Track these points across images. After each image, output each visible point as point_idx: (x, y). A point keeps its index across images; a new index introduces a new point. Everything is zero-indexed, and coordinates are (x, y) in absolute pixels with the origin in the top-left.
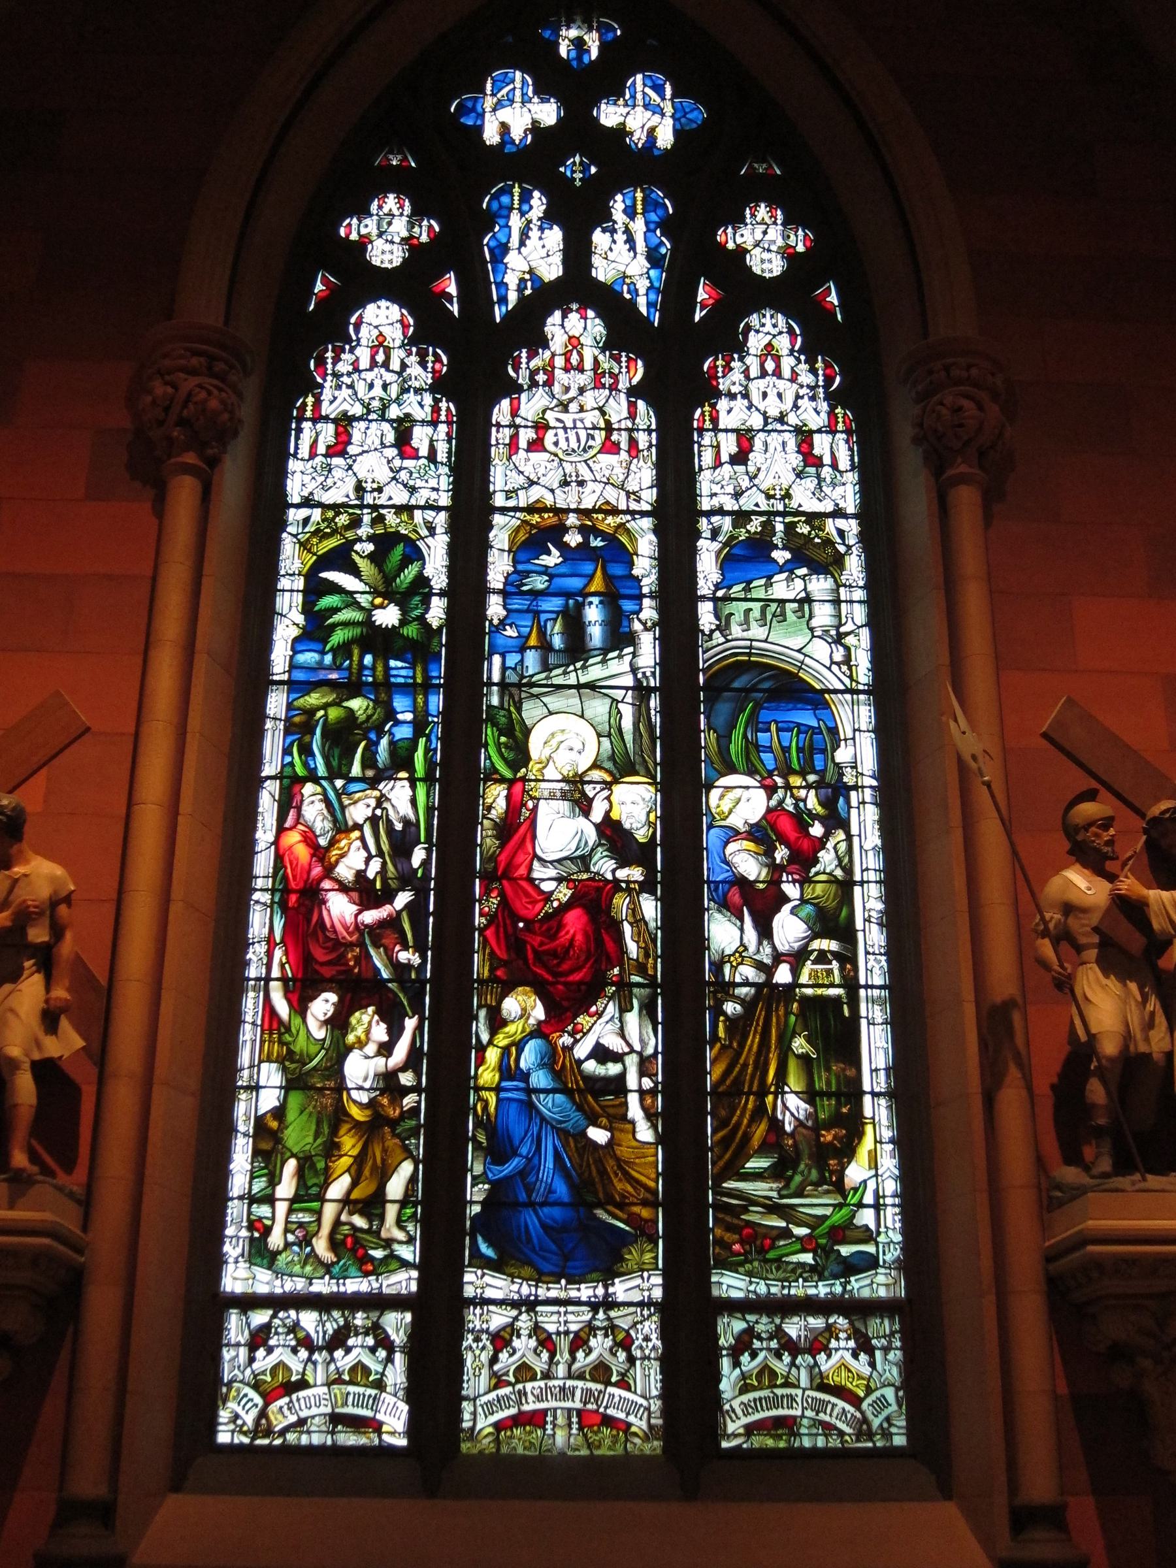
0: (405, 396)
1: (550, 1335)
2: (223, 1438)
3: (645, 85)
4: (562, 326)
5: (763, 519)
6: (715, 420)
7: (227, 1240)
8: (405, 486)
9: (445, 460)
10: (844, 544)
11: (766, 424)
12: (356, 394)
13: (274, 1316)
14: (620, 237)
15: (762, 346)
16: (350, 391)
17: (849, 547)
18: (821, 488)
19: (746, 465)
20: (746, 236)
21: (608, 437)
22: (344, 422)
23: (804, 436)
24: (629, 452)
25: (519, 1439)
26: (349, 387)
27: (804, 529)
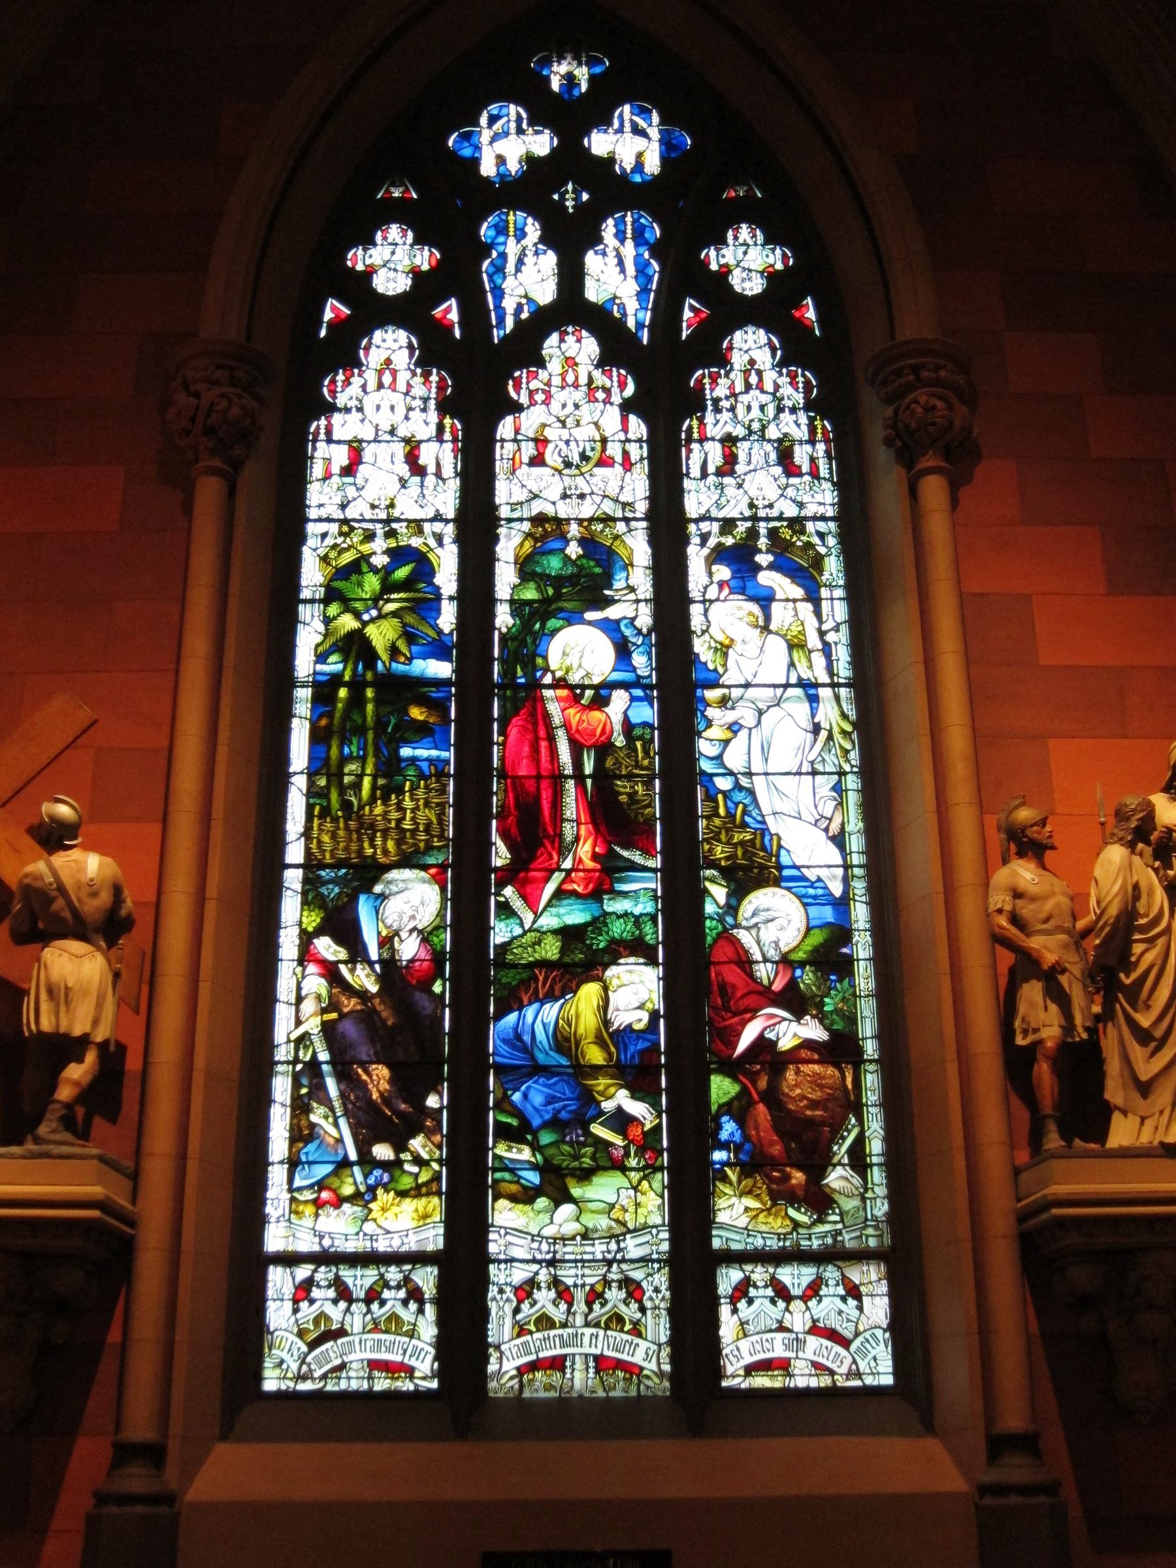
1: (567, 1288)
2: (270, 1385)
3: (632, 113)
4: (559, 347)
6: (329, 431)
7: (269, 1202)
8: (794, 501)
9: (827, 476)
10: (824, 545)
12: (736, 416)
13: (315, 1271)
14: (612, 260)
15: (382, 361)
17: (829, 549)
18: (424, 496)
19: (355, 476)
20: (729, 255)
22: (729, 441)
23: (412, 449)
24: (623, 465)
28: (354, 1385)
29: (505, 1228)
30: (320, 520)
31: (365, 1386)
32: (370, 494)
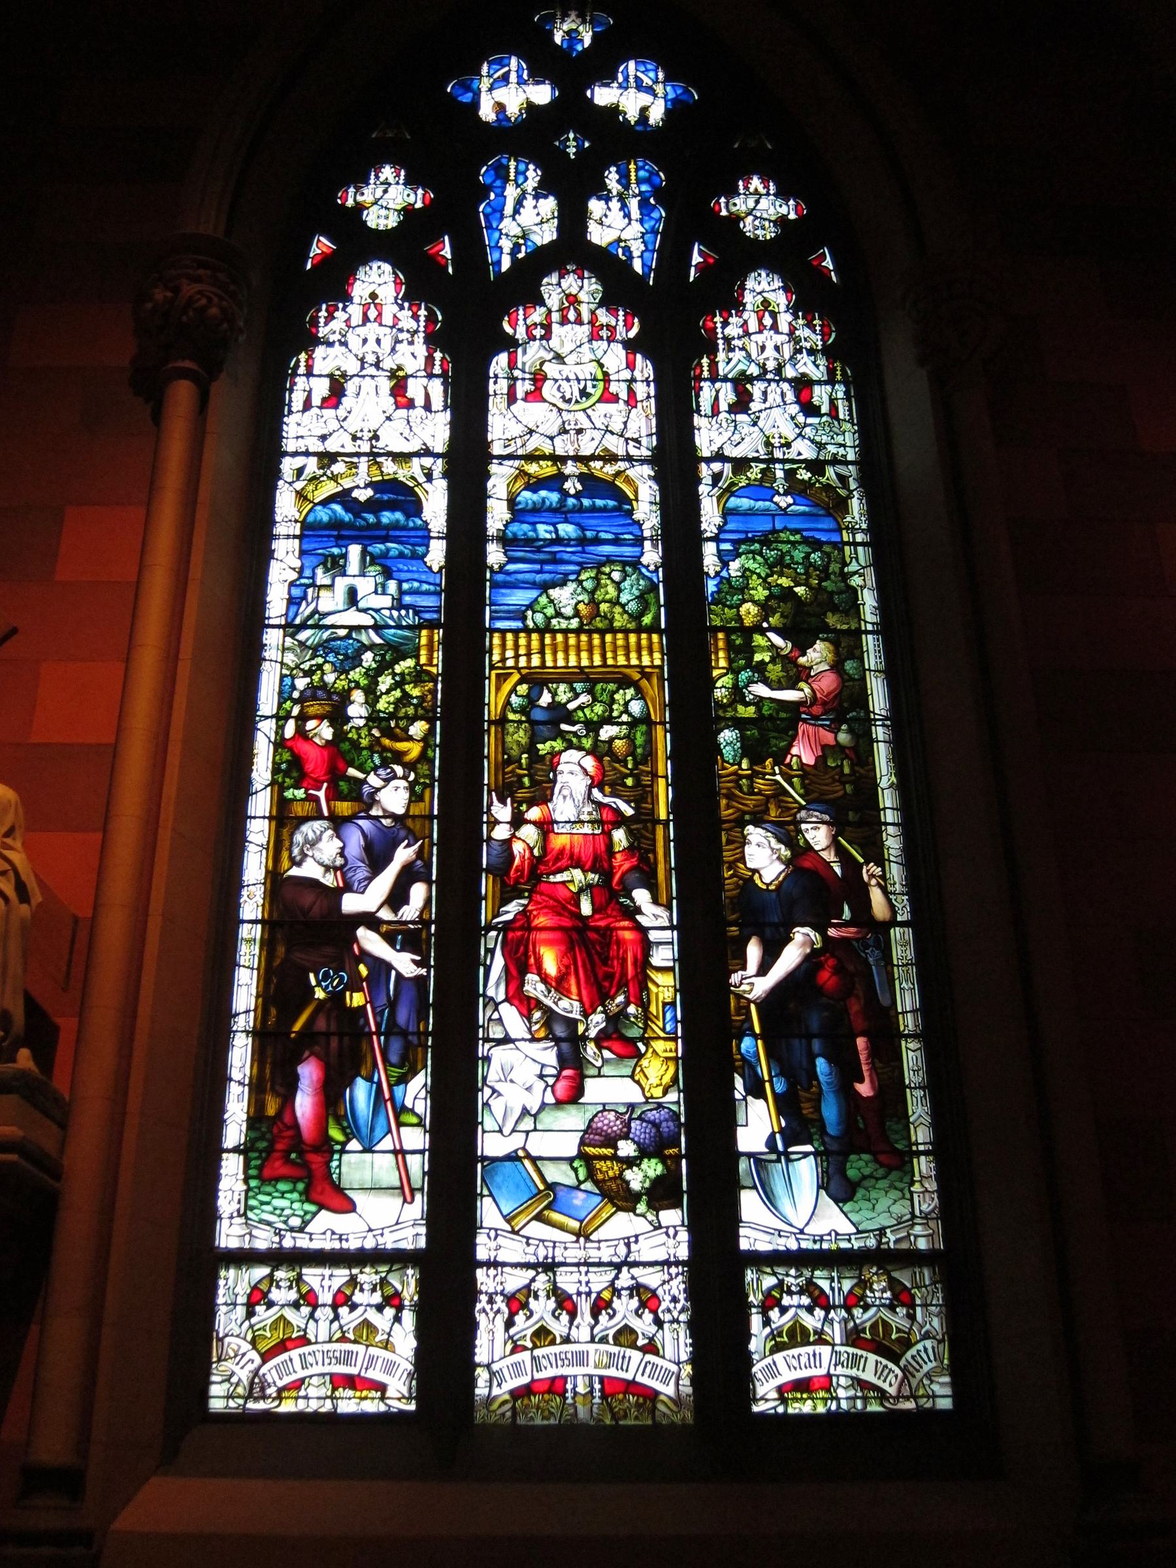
0: (799, 356)
2: (216, 1405)
5: (763, 466)
8: (812, 441)
11: (362, 368)
16: (743, 353)
20: (741, 204)
21: (606, 389)
23: (802, 385)
24: (627, 403)
25: (538, 1408)
26: (741, 349)
27: (804, 475)
28: (314, 1406)
29: (496, 1230)
30: (295, 454)
31: (328, 1406)
32: (353, 425)
